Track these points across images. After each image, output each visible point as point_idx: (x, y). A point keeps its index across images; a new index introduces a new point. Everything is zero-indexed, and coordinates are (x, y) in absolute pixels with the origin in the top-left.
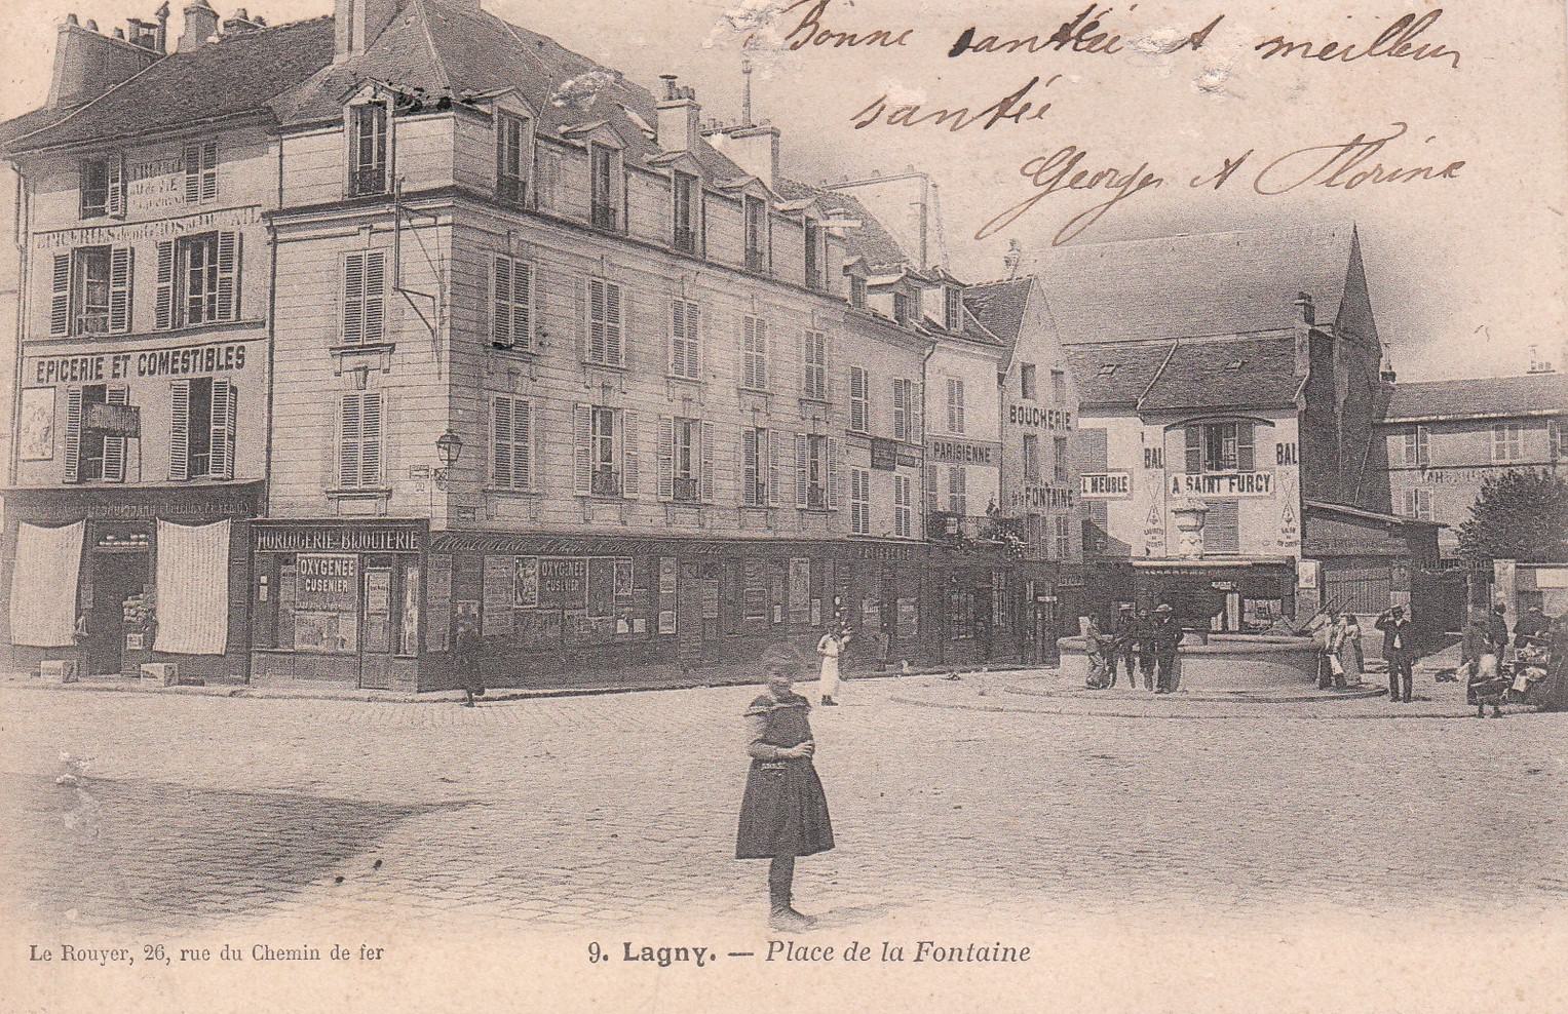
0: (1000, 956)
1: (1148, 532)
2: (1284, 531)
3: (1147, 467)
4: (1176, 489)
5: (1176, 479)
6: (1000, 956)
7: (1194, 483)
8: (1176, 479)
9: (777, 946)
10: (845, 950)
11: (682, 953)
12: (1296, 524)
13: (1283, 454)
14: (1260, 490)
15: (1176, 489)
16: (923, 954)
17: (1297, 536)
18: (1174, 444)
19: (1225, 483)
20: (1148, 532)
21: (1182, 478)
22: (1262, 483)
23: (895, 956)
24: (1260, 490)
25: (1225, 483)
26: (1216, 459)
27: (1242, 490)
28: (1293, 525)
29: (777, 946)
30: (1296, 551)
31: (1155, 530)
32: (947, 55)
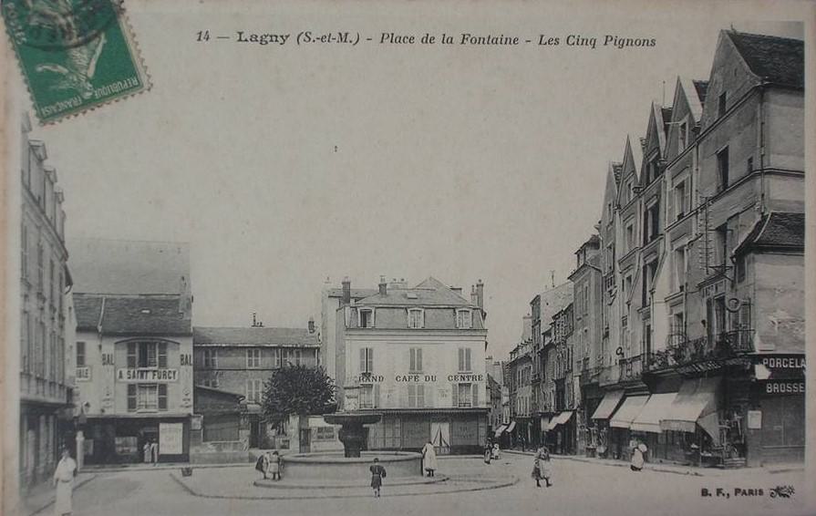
0: (503, 42)
1: (104, 400)
2: (184, 400)
3: (104, 364)
4: (121, 377)
5: (121, 373)
6: (503, 42)
7: (132, 373)
8: (121, 373)
9: (609, 39)
10: (299, 33)
11: (274, 38)
12: (191, 396)
13: (184, 360)
14: (170, 378)
15: (121, 377)
16: (465, 41)
17: (191, 402)
18: (121, 356)
19: (150, 374)
20: (104, 400)
21: (125, 371)
22: (171, 375)
23: (449, 40)
24: (170, 378)
25: (150, 374)
26: (144, 362)
27: (159, 378)
28: (189, 397)
29: (609, 39)
30: (191, 411)
31: (109, 400)
32: (704, 487)
